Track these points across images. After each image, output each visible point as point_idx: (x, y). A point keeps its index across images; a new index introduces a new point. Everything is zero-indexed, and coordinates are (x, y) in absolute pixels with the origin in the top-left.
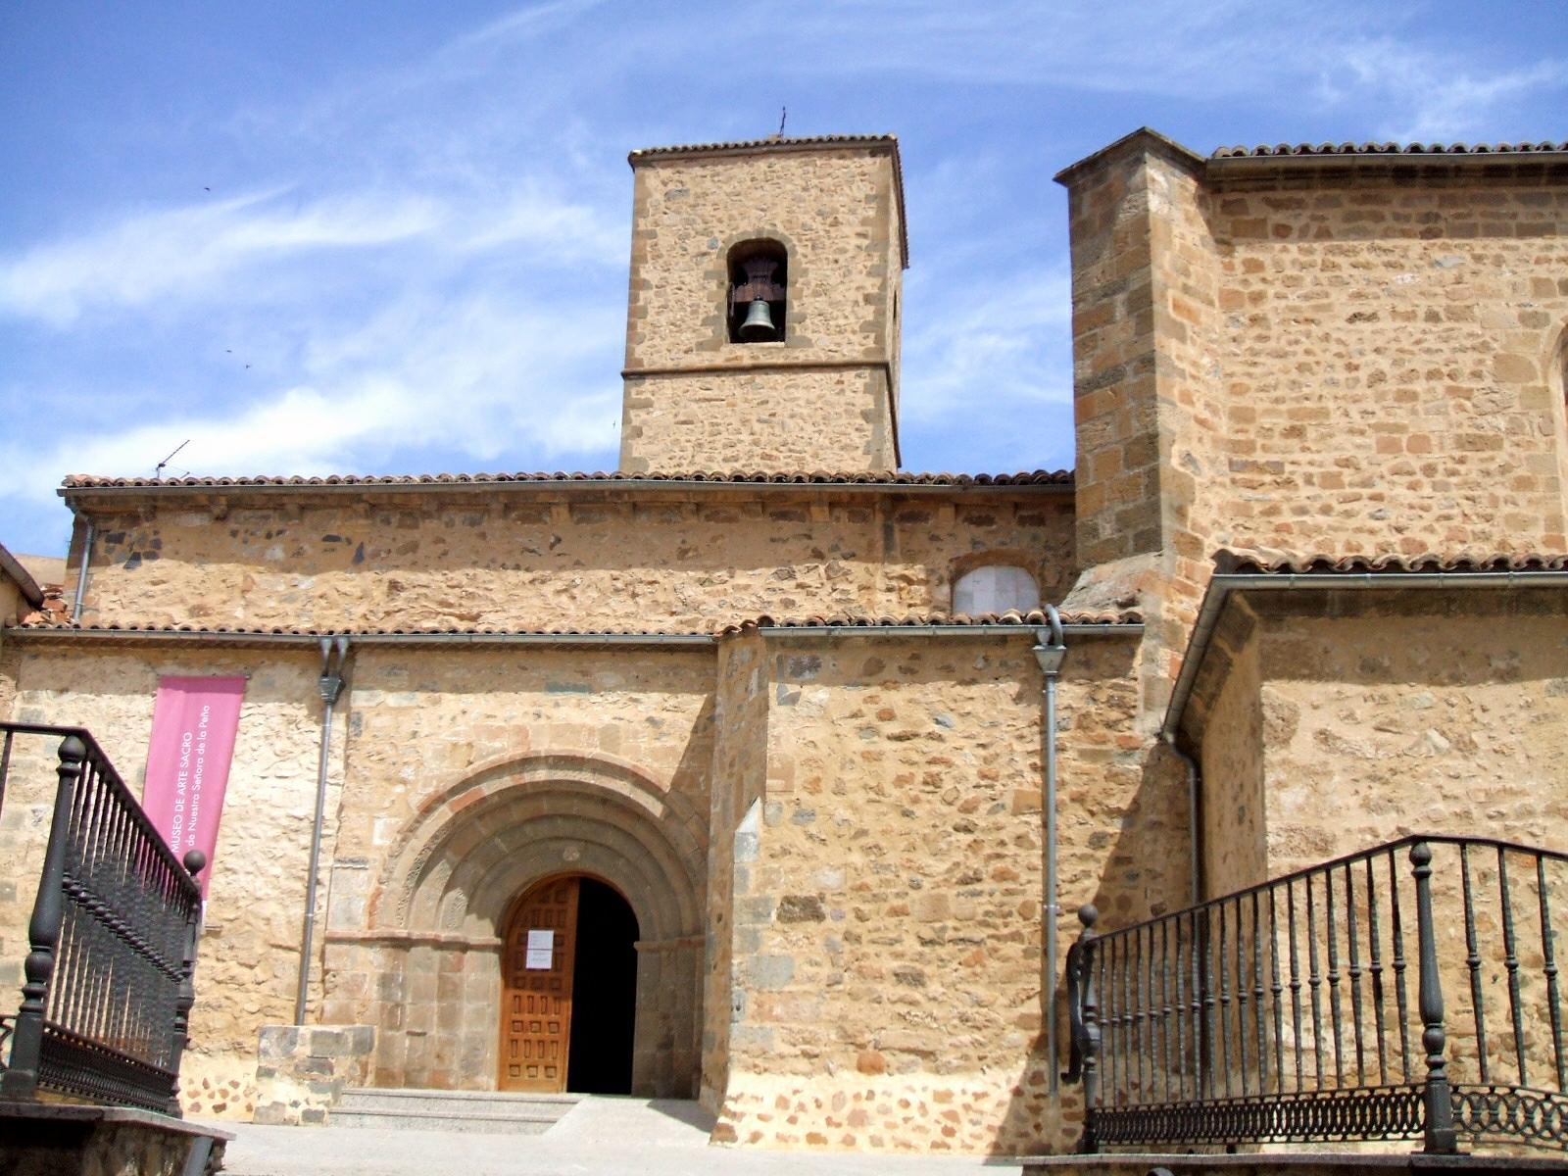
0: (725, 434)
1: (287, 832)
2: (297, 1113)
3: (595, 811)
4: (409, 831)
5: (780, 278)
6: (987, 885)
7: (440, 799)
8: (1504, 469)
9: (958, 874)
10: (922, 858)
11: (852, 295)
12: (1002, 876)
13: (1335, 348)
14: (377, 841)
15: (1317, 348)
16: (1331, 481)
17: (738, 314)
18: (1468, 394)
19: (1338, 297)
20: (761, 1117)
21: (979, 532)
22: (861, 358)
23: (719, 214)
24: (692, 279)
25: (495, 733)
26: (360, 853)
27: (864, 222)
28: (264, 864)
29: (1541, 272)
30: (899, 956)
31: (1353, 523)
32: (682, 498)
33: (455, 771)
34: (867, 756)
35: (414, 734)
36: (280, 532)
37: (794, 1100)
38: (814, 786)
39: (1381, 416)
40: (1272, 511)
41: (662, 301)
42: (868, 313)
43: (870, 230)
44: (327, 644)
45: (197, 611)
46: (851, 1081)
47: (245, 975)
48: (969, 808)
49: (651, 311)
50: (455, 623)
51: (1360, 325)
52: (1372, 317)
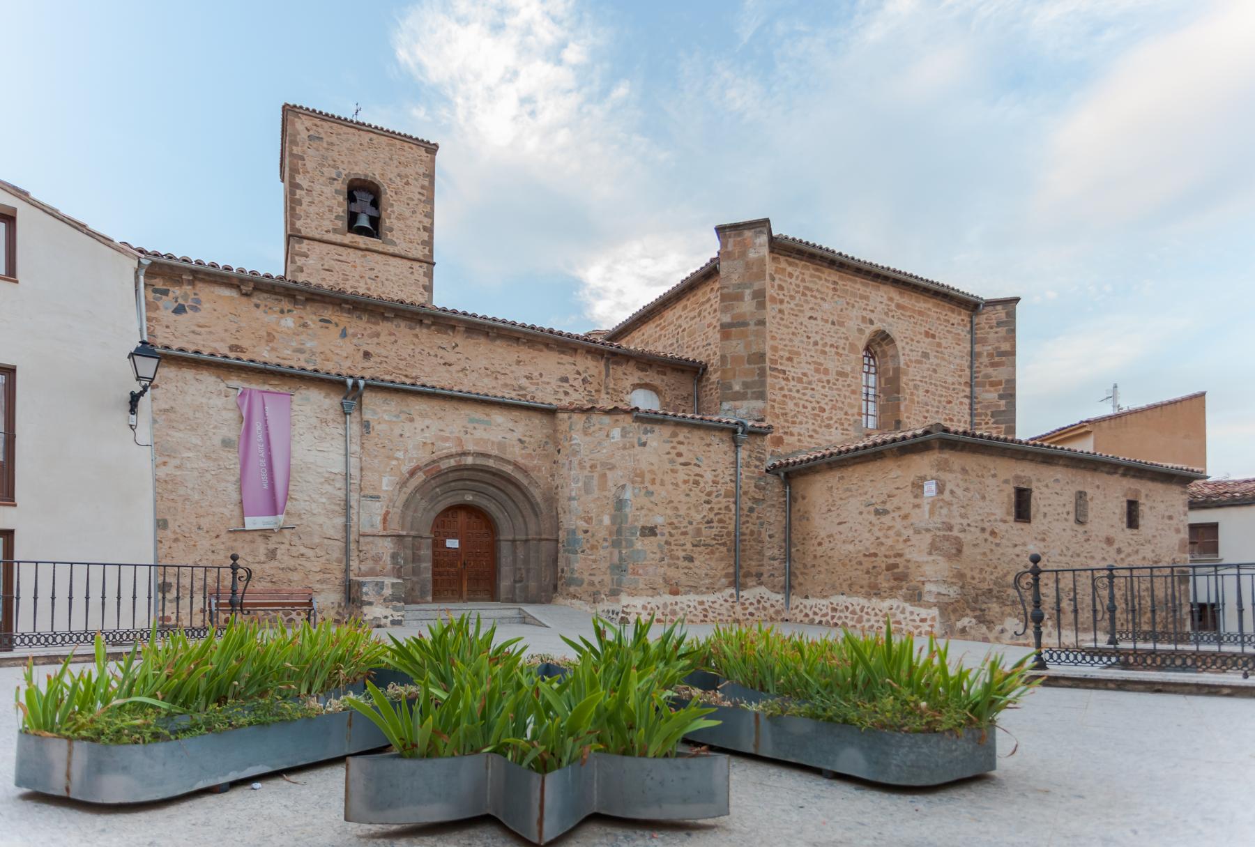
1: (328, 481)
2: (388, 621)
3: (487, 477)
4: (404, 484)
5: (375, 203)
6: (715, 524)
8: (849, 386)
10: (693, 513)
11: (417, 225)
12: (720, 521)
16: (800, 381)
17: (353, 217)
19: (806, 307)
21: (641, 374)
23: (342, 158)
24: (329, 191)
25: (446, 439)
26: (376, 493)
28: (316, 496)
29: (864, 313)
32: (521, 335)
33: (425, 457)
36: (289, 311)
38: (653, 482)
40: (782, 389)
42: (425, 236)
44: (350, 382)
45: (234, 348)
46: (669, 599)
47: (310, 553)
48: (709, 494)
50: (404, 379)
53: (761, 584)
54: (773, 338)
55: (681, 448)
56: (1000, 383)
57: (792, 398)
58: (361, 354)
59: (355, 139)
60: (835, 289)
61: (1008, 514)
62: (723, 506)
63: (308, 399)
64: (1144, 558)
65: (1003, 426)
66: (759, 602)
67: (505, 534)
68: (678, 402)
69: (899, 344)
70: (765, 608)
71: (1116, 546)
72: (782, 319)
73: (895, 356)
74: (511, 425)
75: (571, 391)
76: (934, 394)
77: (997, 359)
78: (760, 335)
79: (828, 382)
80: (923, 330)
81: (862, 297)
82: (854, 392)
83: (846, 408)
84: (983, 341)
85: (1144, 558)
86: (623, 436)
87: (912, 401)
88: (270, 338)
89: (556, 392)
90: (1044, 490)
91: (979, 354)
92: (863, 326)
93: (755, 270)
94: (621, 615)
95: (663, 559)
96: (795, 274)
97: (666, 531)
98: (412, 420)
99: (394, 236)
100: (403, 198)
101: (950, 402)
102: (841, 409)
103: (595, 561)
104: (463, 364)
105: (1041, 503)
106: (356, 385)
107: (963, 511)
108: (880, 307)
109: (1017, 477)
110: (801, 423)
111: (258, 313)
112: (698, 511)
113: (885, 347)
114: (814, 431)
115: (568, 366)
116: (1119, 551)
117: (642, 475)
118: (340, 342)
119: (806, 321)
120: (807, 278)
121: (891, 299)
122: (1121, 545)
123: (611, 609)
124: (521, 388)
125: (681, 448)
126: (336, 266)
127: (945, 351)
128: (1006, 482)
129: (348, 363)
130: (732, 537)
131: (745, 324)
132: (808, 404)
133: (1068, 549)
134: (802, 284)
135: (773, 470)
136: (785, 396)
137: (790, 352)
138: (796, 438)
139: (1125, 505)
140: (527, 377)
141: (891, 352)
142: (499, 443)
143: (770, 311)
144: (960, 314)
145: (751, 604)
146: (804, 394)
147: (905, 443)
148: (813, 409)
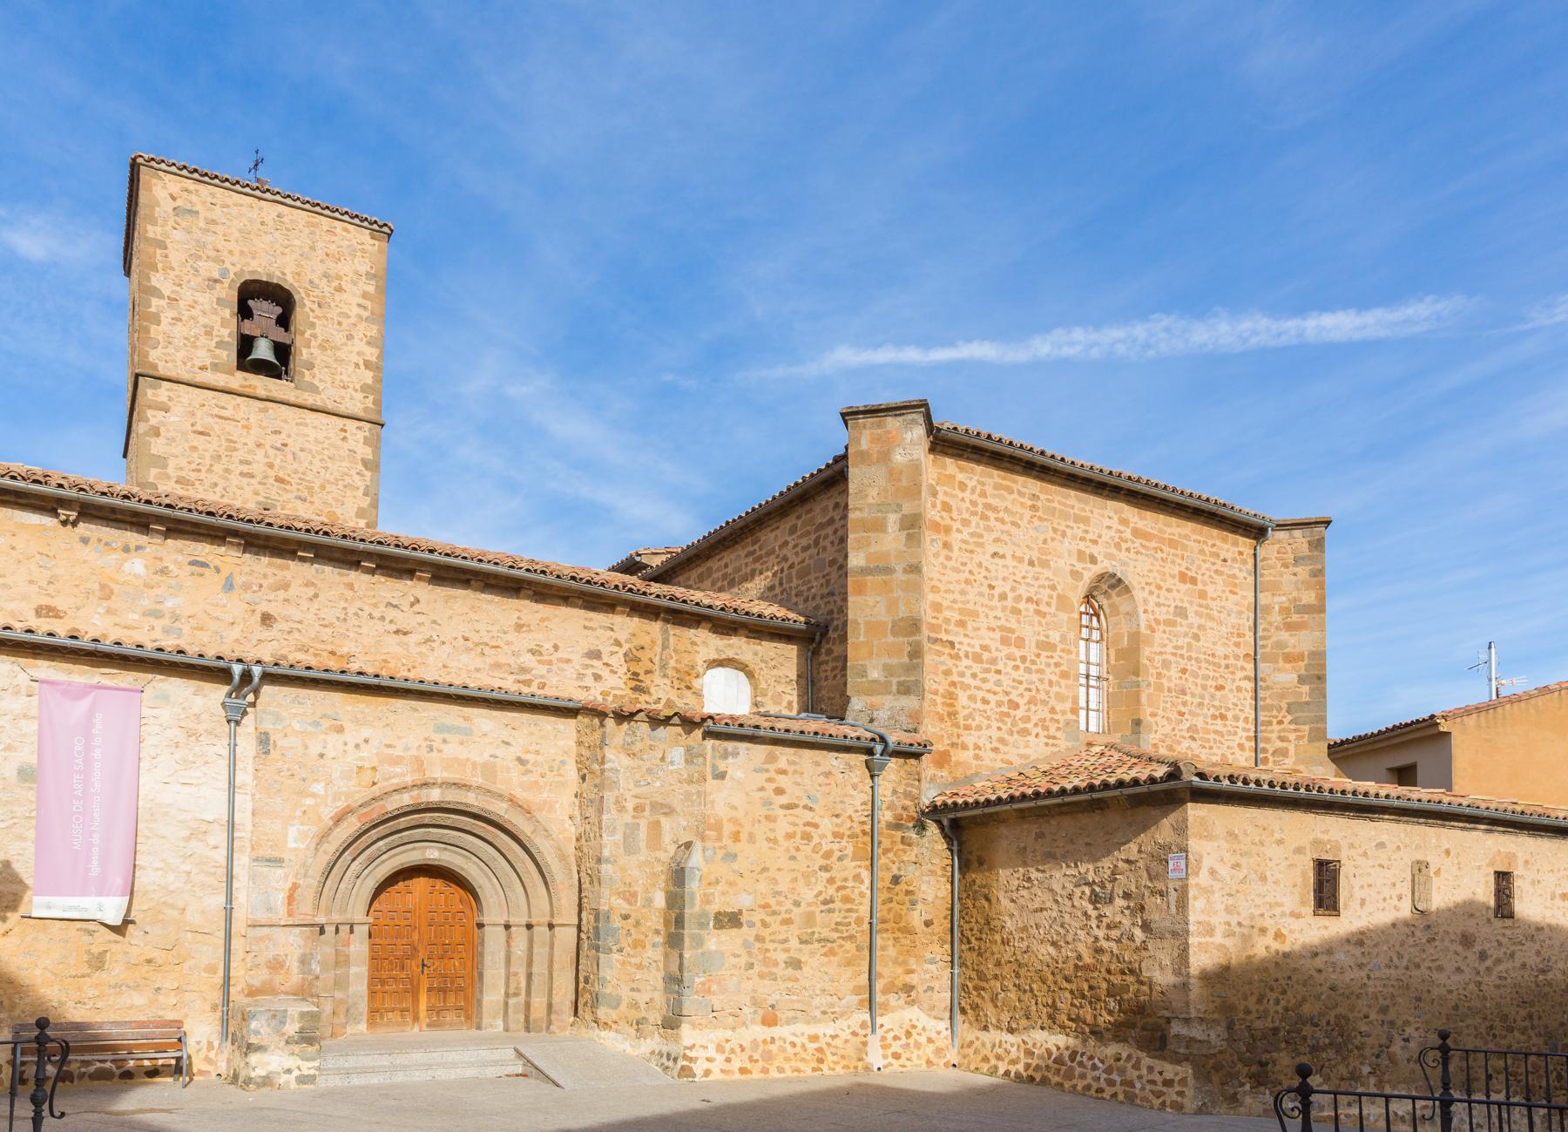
0: (241, 452)
4: (324, 837)
5: (284, 321)
6: (837, 905)
7: (348, 811)
8: (1057, 665)
9: (821, 898)
11: (355, 358)
12: (846, 899)
13: (984, 573)
14: (291, 845)
15: (976, 570)
16: (977, 658)
17: (245, 344)
18: (1044, 615)
19: (988, 538)
20: (708, 1059)
22: (361, 414)
23: (232, 246)
24: (206, 299)
25: (396, 761)
26: (276, 854)
27: (365, 295)
29: (1082, 545)
30: (787, 950)
31: (986, 686)
34: (767, 817)
35: (322, 756)
36: (138, 548)
37: (728, 1046)
38: (736, 837)
39: (1002, 622)
40: (947, 673)
41: (173, 314)
43: (368, 304)
44: (237, 669)
45: (43, 611)
46: (760, 1032)
48: (827, 855)
49: (164, 321)
51: (997, 560)
52: (1003, 557)
53: (911, 1003)
54: (935, 589)
55: (782, 781)
56: (1300, 657)
57: (966, 687)
58: (258, 617)
59: (254, 214)
60: (1033, 508)
61: (1303, 903)
62: (850, 874)
63: (166, 698)
64: (1524, 965)
65: (1307, 728)
66: (908, 1034)
67: (493, 913)
68: (780, 688)
69: (1138, 594)
70: (918, 1045)
71: (1477, 948)
72: (949, 558)
73: (1132, 615)
74: (505, 734)
75: (605, 672)
76: (1195, 675)
77: (1295, 618)
78: (915, 588)
79: (1024, 659)
80: (1176, 570)
81: (1078, 519)
82: (1065, 675)
83: (1053, 702)
84: (1275, 587)
85: (1524, 965)
86: (689, 761)
87: (1160, 687)
88: (106, 593)
89: (581, 676)
90: (1361, 861)
91: (1268, 609)
92: (1079, 566)
93: (905, 483)
94: (682, 1062)
95: (751, 966)
96: (971, 484)
97: (757, 917)
98: (340, 730)
99: (318, 377)
100: (333, 314)
101: (1220, 688)
102: (1044, 703)
103: (640, 967)
104: (427, 631)
105: (1356, 883)
106: (247, 677)
107: (1231, 901)
108: (1107, 535)
109: (1316, 842)
110: (979, 728)
111: (87, 553)
112: (808, 884)
113: (1115, 599)
114: (1002, 740)
115: (600, 632)
116: (1483, 956)
117: (718, 827)
118: (223, 598)
119: (986, 559)
120: (989, 490)
121: (1124, 522)
122: (1487, 946)
123: (665, 1049)
124: (524, 670)
125: (782, 781)
126: (217, 425)
127: (1213, 604)
128: (1299, 850)
129: (235, 633)
130: (866, 926)
131: (888, 570)
132: (990, 697)
133: (1400, 956)
134: (981, 501)
135: (935, 811)
136: (953, 684)
137: (961, 611)
138: (971, 753)
139: (1492, 879)
140: (532, 652)
141: (1124, 607)
142: (485, 766)
143: (931, 545)
144: (1235, 544)
145: (896, 1038)
146: (984, 680)
147: (1137, 790)
148: (999, 704)
